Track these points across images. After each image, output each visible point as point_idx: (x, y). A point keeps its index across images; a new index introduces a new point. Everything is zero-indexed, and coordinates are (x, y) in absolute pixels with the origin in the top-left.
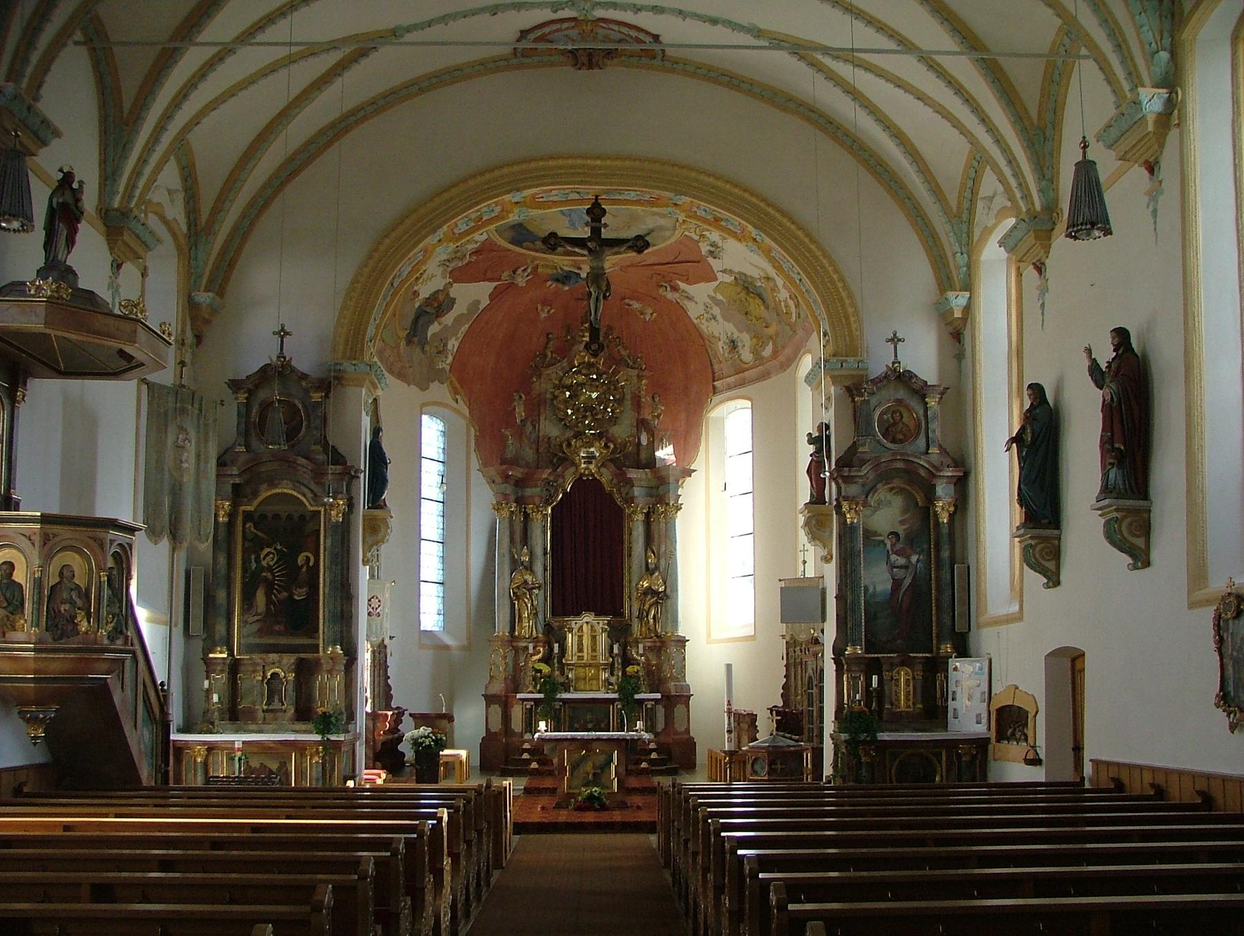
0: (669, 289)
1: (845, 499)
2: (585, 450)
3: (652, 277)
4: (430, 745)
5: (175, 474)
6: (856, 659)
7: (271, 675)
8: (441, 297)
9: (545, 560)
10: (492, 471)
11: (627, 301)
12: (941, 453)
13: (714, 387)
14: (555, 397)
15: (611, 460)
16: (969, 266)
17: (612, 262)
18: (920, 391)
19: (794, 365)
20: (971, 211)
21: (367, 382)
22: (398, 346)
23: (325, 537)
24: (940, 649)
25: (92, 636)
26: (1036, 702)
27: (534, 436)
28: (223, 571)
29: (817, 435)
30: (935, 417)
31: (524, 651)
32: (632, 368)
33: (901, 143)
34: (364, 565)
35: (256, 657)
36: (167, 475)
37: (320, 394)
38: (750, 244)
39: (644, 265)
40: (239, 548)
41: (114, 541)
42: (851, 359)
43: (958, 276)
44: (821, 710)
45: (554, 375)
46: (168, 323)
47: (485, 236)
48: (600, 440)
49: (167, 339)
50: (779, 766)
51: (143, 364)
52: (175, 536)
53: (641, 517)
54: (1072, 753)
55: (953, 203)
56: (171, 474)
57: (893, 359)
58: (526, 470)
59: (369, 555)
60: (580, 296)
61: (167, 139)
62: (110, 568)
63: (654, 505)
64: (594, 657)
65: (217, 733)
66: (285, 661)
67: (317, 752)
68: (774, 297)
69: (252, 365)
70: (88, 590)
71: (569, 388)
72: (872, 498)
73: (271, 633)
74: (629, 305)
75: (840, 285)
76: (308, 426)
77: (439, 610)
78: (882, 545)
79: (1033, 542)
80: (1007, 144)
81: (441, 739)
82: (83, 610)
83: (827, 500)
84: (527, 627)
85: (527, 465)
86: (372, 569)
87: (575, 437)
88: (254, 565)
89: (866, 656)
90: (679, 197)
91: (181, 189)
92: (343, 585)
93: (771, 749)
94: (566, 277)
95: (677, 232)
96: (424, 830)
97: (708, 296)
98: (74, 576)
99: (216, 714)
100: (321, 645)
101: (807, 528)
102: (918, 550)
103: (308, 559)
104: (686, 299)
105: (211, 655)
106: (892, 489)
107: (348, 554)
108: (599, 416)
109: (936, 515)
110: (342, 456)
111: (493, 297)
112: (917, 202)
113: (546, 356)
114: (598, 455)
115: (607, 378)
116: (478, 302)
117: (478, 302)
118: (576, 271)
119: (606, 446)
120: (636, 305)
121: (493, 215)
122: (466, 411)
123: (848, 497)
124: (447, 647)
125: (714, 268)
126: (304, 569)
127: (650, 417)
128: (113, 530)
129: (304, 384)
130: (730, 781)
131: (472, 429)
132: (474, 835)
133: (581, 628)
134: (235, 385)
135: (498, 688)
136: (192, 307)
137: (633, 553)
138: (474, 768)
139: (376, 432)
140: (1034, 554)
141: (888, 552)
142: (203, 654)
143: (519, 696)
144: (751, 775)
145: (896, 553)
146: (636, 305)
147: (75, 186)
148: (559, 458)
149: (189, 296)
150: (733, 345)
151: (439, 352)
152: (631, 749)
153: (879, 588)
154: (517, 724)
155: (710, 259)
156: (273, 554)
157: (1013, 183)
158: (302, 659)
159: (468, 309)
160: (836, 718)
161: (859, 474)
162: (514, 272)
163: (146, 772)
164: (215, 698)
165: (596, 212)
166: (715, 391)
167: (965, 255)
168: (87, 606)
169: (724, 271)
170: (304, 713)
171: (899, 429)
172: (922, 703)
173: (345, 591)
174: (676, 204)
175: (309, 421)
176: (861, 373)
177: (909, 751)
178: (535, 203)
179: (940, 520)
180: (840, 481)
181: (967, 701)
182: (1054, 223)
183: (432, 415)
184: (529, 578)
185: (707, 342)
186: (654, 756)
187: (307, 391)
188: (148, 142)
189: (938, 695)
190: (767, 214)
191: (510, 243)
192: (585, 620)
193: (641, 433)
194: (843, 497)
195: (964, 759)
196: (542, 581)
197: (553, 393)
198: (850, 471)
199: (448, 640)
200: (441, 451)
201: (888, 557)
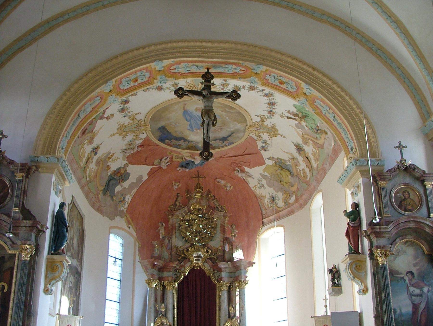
0: (239, 171)
1: (378, 247)
3: (231, 165)
8: (122, 171)
9: (174, 311)
10: (146, 262)
11: (218, 180)
13: (263, 222)
14: (181, 226)
17: (218, 101)
19: (308, 204)
21: (56, 171)
22: (98, 195)
29: (351, 210)
32: (221, 211)
33: (398, 27)
37: (22, 174)
38: (302, 98)
45: (180, 215)
48: (204, 248)
53: (225, 288)
58: (164, 262)
60: (194, 176)
68: (296, 169)
72: (394, 247)
74: (219, 182)
75: (361, 116)
87: (191, 246)
92: (25, 306)
94: (187, 164)
95: (246, 133)
102: (427, 284)
104: (248, 177)
106: (406, 243)
108: (204, 236)
111: (151, 174)
113: (176, 205)
114: (202, 256)
116: (142, 177)
117: (142, 177)
118: (193, 160)
119: (207, 252)
120: (223, 182)
122: (134, 234)
123: (380, 246)
125: (264, 157)
131: (137, 243)
137: (221, 309)
145: (413, 285)
146: (223, 182)
150: (273, 199)
151: (121, 201)
153: (404, 310)
159: (137, 180)
162: (161, 160)
166: (263, 224)
169: (269, 159)
171: (408, 203)
174: (256, 73)
183: (117, 234)
184: (164, 321)
185: (259, 199)
187: (13, 173)
190: (313, 75)
191: (159, 140)
193: (225, 244)
197: (180, 224)
198: (380, 229)
200: (120, 254)
201: (408, 288)
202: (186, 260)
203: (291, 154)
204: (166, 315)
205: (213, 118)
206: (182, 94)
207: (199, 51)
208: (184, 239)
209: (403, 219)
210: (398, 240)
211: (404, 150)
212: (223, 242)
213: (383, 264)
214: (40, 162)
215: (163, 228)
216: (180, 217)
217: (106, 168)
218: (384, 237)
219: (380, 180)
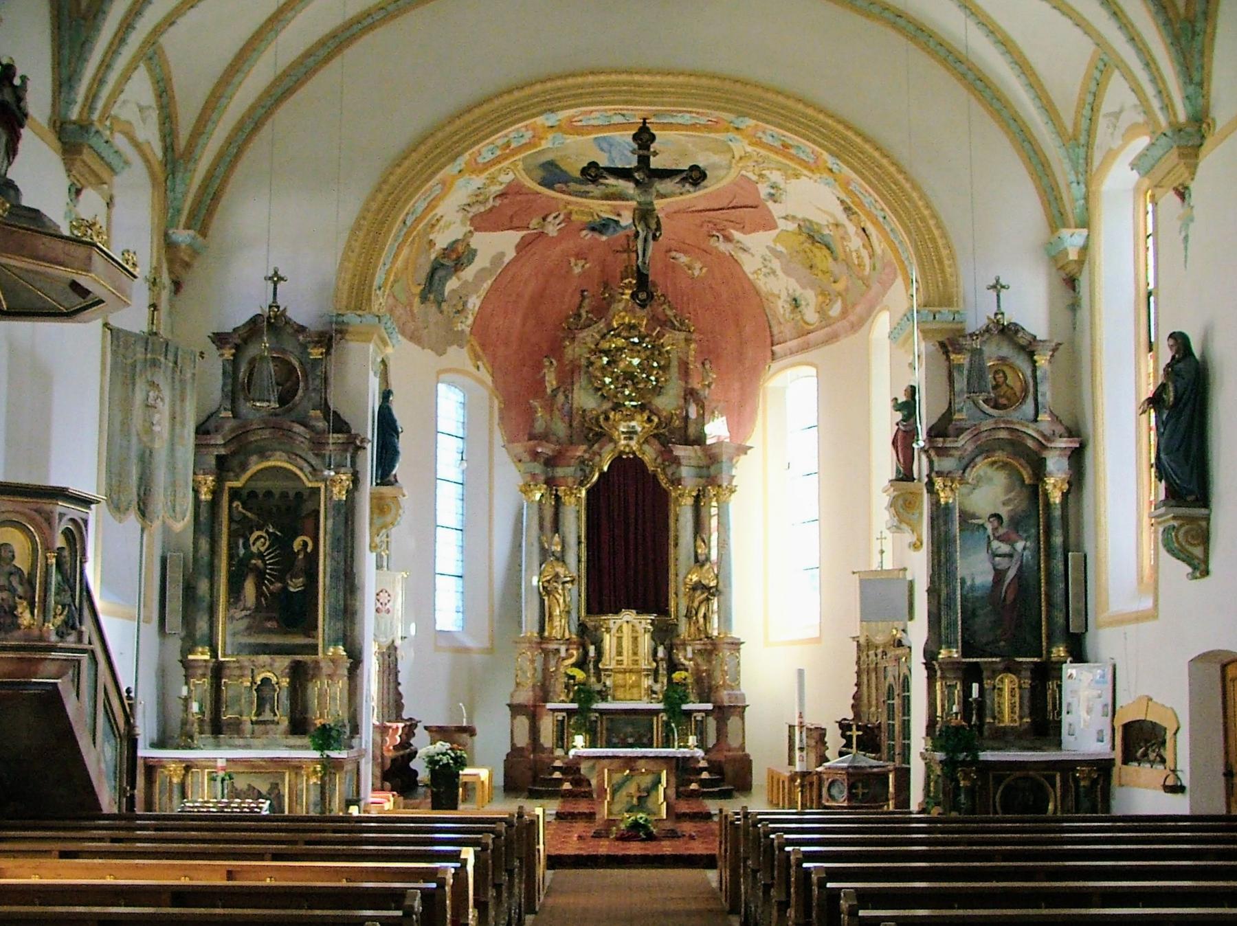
1: (939, 474)
2: (625, 424)
4: (448, 763)
5: (145, 439)
6: (952, 665)
7: (262, 680)
8: (460, 248)
10: (519, 448)
11: (673, 254)
12: (1052, 420)
13: (773, 353)
14: (591, 364)
15: (655, 436)
16: (1086, 198)
18: (1029, 349)
19: (867, 325)
20: (1090, 133)
21: (375, 336)
22: (411, 305)
23: (326, 518)
24: (1051, 652)
25: (36, 632)
26: (1177, 717)
27: (567, 407)
28: (206, 559)
30: (1044, 377)
31: (555, 655)
32: (680, 330)
34: (372, 551)
35: (245, 659)
36: (134, 440)
38: (825, 175)
39: (693, 211)
40: (225, 530)
41: (65, 514)
42: (945, 310)
43: (1073, 208)
44: (906, 726)
45: (589, 339)
46: (131, 251)
47: (511, 176)
49: (131, 270)
50: (860, 791)
51: (101, 301)
52: (143, 512)
53: (688, 501)
54: (1222, 779)
55: (1068, 121)
56: (140, 440)
57: (995, 310)
58: (558, 447)
59: (377, 540)
60: (620, 248)
61: (135, 40)
62: (58, 549)
63: (705, 487)
64: (636, 662)
65: (198, 748)
66: (277, 665)
67: (315, 772)
68: (844, 247)
69: (237, 316)
70: (32, 575)
71: (607, 352)
73: (262, 631)
75: (932, 222)
76: (306, 389)
77: (457, 607)
78: (981, 529)
79: (1176, 523)
80: (1145, 44)
81: (461, 757)
82: (25, 599)
83: (916, 476)
84: (560, 627)
85: (558, 442)
86: (379, 557)
87: (613, 409)
88: (242, 552)
89: (964, 660)
90: (741, 119)
91: (154, 106)
92: (346, 574)
93: (850, 770)
94: (604, 225)
95: (733, 170)
96: (445, 879)
97: (767, 247)
98: (13, 556)
99: (196, 725)
100: (320, 646)
101: (892, 510)
102: (1025, 535)
103: (305, 544)
105: (191, 657)
106: (993, 463)
107: (353, 537)
108: (641, 386)
109: (1046, 494)
110: (346, 423)
111: (522, 247)
112: (1024, 123)
113: (580, 316)
115: (649, 342)
116: (502, 254)
117: (502, 254)
118: (616, 218)
119: (649, 420)
120: (683, 259)
121: (523, 141)
122: (488, 379)
124: (466, 650)
126: (301, 557)
127: (697, 386)
128: (64, 501)
129: (301, 338)
130: (804, 806)
132: (505, 878)
133: (620, 629)
134: (220, 339)
135: (525, 696)
136: (169, 246)
138: (494, 788)
139: (386, 395)
140: (1176, 536)
141: (989, 537)
142: (182, 656)
143: (549, 706)
144: (828, 801)
145: (998, 538)
146: (683, 259)
147: (17, 82)
148: (595, 433)
149: (166, 235)
150: (796, 303)
151: (458, 312)
152: (683, 768)
154: (547, 736)
155: (770, 204)
156: (265, 538)
157: (1150, 90)
158: (299, 662)
159: (492, 263)
160: (927, 735)
161: (955, 445)
162: (544, 219)
163: (108, 800)
164: (195, 707)
165: (644, 137)
167: (1082, 186)
168: (29, 594)
169: (785, 218)
170: (299, 726)
172: (1031, 715)
173: (348, 580)
174: (737, 129)
175: (306, 381)
176: (959, 326)
177: (1018, 774)
178: (573, 128)
179: (1052, 500)
180: (932, 453)
181: (1085, 715)
182: (1203, 137)
184: (561, 570)
186: (705, 775)
187: (304, 347)
188: (111, 44)
189: (1050, 707)
190: (845, 139)
191: (539, 184)
192: (625, 618)
194: (937, 472)
195: (1082, 783)
196: (575, 574)
197: (588, 358)
199: (469, 642)
200: (460, 425)
201: (989, 543)
202: (604, 439)
203: (832, 215)
204: (563, 556)
205: (654, 226)
206: (596, 175)
207: (626, 92)
208: (600, 393)
209: (987, 425)
210: (978, 459)
211: (1003, 293)
212: (685, 399)
213: (947, 503)
214: (348, 324)
215: (552, 369)
216: (589, 345)
217: (427, 247)
218: (951, 456)
219: (954, 353)
